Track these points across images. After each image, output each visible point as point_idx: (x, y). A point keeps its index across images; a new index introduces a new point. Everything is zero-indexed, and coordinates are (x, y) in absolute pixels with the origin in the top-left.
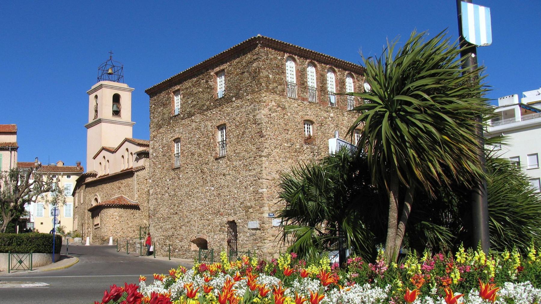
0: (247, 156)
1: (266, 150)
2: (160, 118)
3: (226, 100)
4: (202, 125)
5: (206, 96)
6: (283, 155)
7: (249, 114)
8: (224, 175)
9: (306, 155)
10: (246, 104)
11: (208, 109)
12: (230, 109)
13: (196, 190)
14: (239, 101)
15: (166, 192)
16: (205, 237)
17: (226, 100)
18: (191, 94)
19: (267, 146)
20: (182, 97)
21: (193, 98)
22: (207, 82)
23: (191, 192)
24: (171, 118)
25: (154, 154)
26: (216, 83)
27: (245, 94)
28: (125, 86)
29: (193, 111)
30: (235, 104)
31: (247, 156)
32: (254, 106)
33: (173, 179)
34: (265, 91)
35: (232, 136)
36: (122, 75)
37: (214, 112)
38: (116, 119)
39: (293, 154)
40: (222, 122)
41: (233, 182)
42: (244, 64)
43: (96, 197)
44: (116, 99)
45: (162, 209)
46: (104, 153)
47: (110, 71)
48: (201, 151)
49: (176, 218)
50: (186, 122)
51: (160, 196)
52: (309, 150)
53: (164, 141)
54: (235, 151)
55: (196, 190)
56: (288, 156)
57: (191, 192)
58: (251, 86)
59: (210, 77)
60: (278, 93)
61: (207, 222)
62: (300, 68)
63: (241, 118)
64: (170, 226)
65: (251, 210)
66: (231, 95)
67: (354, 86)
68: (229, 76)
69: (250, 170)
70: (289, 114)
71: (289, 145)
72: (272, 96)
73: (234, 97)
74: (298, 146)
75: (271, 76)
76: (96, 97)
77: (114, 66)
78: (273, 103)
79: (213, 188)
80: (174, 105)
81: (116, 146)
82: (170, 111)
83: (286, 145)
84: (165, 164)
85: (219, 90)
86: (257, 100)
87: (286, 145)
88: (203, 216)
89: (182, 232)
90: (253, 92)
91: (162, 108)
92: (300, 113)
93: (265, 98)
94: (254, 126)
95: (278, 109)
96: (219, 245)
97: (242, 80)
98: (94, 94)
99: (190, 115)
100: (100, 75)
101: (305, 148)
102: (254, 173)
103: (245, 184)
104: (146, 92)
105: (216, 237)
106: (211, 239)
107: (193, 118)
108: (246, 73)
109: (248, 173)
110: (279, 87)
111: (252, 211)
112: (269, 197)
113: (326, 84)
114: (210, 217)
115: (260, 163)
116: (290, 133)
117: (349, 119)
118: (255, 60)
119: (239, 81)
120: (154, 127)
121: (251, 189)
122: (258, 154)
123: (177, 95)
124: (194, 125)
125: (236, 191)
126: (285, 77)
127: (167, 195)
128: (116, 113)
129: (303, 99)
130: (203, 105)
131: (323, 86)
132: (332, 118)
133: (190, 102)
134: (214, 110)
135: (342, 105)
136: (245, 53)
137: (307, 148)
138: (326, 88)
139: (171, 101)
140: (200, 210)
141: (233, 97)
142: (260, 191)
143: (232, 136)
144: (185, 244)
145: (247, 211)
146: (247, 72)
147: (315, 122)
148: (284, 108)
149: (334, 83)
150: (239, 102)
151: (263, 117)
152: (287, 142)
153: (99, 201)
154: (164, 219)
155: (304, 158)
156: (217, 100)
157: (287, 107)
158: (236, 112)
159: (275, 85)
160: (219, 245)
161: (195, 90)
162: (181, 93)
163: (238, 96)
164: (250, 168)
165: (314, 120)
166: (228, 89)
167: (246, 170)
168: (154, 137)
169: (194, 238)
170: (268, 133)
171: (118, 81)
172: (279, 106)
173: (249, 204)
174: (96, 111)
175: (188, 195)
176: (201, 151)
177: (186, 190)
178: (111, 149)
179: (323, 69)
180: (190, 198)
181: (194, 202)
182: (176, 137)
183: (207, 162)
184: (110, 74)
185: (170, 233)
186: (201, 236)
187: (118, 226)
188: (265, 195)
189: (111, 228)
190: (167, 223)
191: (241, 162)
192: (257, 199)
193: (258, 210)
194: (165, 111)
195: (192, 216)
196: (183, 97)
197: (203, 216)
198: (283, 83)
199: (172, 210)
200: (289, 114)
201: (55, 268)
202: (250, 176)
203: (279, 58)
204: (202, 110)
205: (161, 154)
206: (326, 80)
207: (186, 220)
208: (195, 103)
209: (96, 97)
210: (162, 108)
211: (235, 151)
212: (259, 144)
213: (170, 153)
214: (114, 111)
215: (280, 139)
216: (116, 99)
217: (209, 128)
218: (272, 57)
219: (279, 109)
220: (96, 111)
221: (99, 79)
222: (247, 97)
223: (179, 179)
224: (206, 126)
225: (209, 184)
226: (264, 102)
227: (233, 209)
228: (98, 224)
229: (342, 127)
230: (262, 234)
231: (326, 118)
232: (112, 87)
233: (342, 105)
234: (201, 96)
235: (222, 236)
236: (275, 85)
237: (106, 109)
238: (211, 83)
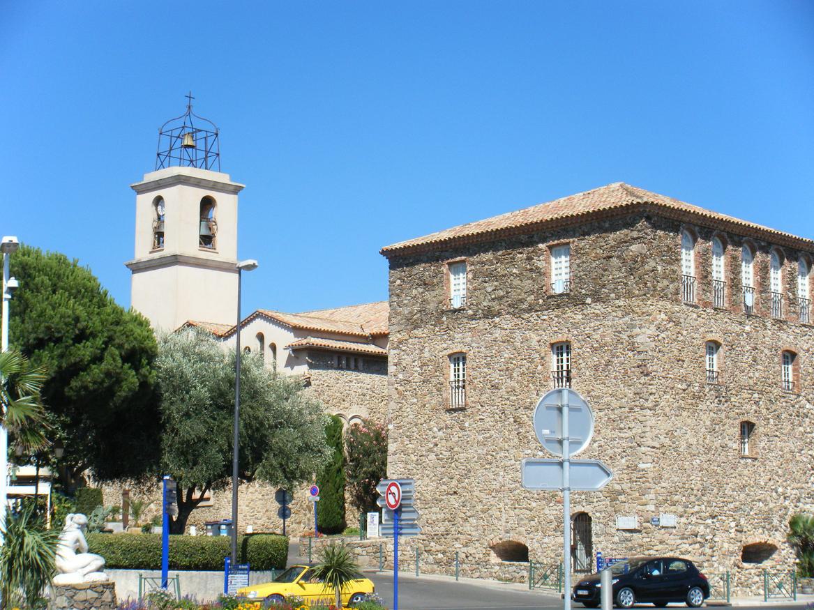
0: (614, 403)
1: (652, 398)
2: (416, 308)
3: (571, 299)
4: (518, 335)
5: (527, 284)
6: (676, 405)
7: (620, 333)
9: (708, 403)
10: (614, 314)
11: (530, 309)
12: (580, 317)
13: (502, 454)
14: (599, 306)
15: (430, 450)
16: (522, 540)
17: (571, 299)
18: (491, 276)
19: (654, 391)
20: (470, 276)
21: (496, 283)
22: (529, 259)
24: (443, 312)
25: (401, 376)
26: (549, 263)
29: (497, 308)
30: (589, 311)
31: (614, 403)
32: (632, 320)
33: (447, 428)
34: (652, 295)
35: (583, 365)
36: (214, 149)
37: (545, 317)
38: (205, 255)
39: (690, 401)
40: (561, 337)
42: (613, 243)
49: (454, 501)
50: (482, 324)
53: (427, 354)
54: (589, 392)
55: (502, 454)
56: (683, 406)
57: (489, 457)
58: (626, 284)
59: (538, 253)
60: (670, 296)
61: (528, 512)
63: (603, 337)
64: (441, 516)
65: (622, 498)
66: (583, 292)
68: (579, 258)
69: (621, 429)
71: (684, 386)
73: (589, 296)
74: (697, 388)
75: (659, 268)
76: (158, 201)
78: (663, 316)
80: (448, 288)
82: (441, 298)
83: (679, 386)
84: (428, 398)
85: (554, 279)
86: (637, 310)
88: (518, 501)
89: (467, 528)
90: (629, 295)
91: (421, 290)
93: (652, 307)
94: (630, 354)
95: (670, 325)
96: (553, 556)
97: (606, 270)
101: (707, 390)
102: (629, 434)
103: (610, 452)
104: (383, 253)
105: (546, 540)
106: (537, 545)
107: (497, 320)
109: (616, 434)
110: (671, 286)
111: (624, 499)
112: (655, 477)
114: (534, 504)
115: (641, 419)
116: (685, 366)
117: (773, 334)
118: (634, 239)
119: (600, 271)
120: (399, 324)
121: (623, 461)
122: (637, 403)
123: (456, 273)
124: (498, 333)
126: (680, 267)
127: (432, 456)
129: (706, 305)
130: (521, 301)
131: (735, 278)
132: (747, 333)
133: (489, 289)
134: (545, 312)
136: (613, 229)
137: (710, 390)
141: (587, 296)
142: (642, 466)
143: (583, 365)
144: (477, 550)
146: (618, 257)
147: (723, 343)
150: (599, 308)
155: (706, 408)
156: (551, 297)
157: (682, 320)
158: (592, 325)
160: (553, 556)
161: (501, 269)
162: (469, 268)
163: (597, 298)
164: (622, 426)
165: (721, 341)
166: (576, 279)
167: (613, 429)
168: (400, 342)
169: (496, 541)
172: (670, 320)
175: (485, 462)
176: (514, 384)
177: (479, 452)
180: (488, 466)
181: (497, 474)
182: (455, 351)
183: (527, 404)
185: (441, 529)
186: (514, 537)
190: (434, 510)
191: (601, 414)
192: (635, 479)
193: (637, 499)
194: (428, 296)
195: (493, 501)
196: (474, 278)
197: (518, 501)
198: (674, 278)
199: (445, 487)
200: (685, 333)
201: (431, 579)
202: (621, 438)
204: (516, 309)
205: (417, 378)
207: (479, 507)
208: (501, 293)
209: (158, 201)
210: (421, 290)
211: (589, 392)
212: (640, 386)
213: (441, 379)
217: (534, 344)
221: (163, 159)
222: (617, 302)
223: (463, 429)
225: (533, 446)
226: (650, 315)
230: (645, 540)
231: (738, 335)
232: (198, 183)
234: (516, 282)
236: (666, 282)
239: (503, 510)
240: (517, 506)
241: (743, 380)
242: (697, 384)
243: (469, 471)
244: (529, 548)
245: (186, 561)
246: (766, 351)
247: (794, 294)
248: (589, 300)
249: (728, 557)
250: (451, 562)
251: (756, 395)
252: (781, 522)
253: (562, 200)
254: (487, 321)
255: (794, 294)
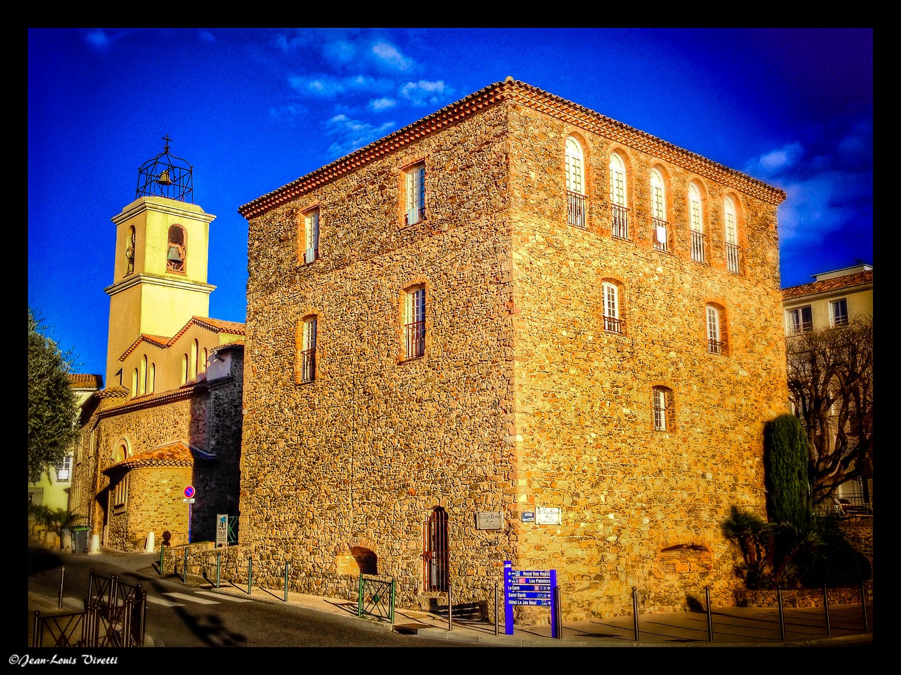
2: (271, 270)
6: (559, 358)
8: (419, 401)
11: (384, 248)
12: (435, 250)
22: (382, 188)
23: (338, 439)
27: (473, 215)
28: (197, 209)
37: (398, 257)
41: (442, 416)
42: (472, 147)
43: (123, 442)
44: (177, 235)
45: (270, 476)
46: (144, 347)
47: (164, 178)
48: (365, 346)
51: (265, 446)
52: (613, 346)
57: (338, 439)
60: (548, 213)
62: (594, 161)
65: (485, 485)
66: (440, 217)
67: (705, 208)
70: (571, 263)
72: (535, 222)
74: (590, 338)
75: (533, 175)
77: (173, 167)
78: (539, 238)
79: (392, 432)
81: (171, 334)
87: (564, 333)
91: (276, 248)
92: (596, 263)
93: (521, 224)
98: (129, 223)
99: (341, 263)
100: (142, 184)
107: (348, 269)
108: (475, 167)
109: (475, 399)
110: (550, 200)
111: (486, 488)
112: (527, 455)
113: (648, 200)
125: (448, 440)
126: (564, 179)
127: (282, 444)
128: (177, 264)
135: (680, 249)
137: (609, 342)
138: (648, 211)
139: (298, 231)
140: (361, 480)
145: (474, 487)
148: (561, 250)
149: (663, 200)
151: (516, 267)
152: (567, 328)
153: (130, 451)
154: (274, 499)
155: (603, 365)
159: (542, 195)
163: (453, 220)
164: (484, 386)
170: (528, 305)
171: (181, 197)
172: (550, 245)
173: (479, 471)
174: (132, 260)
176: (365, 346)
178: (160, 341)
179: (645, 165)
184: (163, 183)
187: (168, 509)
188: (519, 447)
189: (152, 513)
200: (571, 263)
203: (552, 135)
206: (649, 192)
210: (276, 248)
214: (171, 261)
215: (552, 318)
216: (177, 235)
218: (536, 132)
219: (551, 250)
220: (132, 260)
221: (140, 193)
222: (477, 222)
224: (378, 287)
227: (440, 481)
228: (122, 505)
229: (680, 296)
233: (680, 249)
235: (412, 545)
236: (542, 195)
237: (155, 255)
238: (390, 191)
239: (350, 506)
240: (365, 501)
241: (654, 331)
242: (590, 333)
243: (318, 459)
244: (378, 556)
245: (774, 499)
246: (686, 301)
247: (719, 236)
248: (446, 227)
249: (640, 565)
250: (290, 576)
251: (673, 354)
252: (712, 516)
253: (871, 598)
254: (338, 272)
255: (719, 236)
